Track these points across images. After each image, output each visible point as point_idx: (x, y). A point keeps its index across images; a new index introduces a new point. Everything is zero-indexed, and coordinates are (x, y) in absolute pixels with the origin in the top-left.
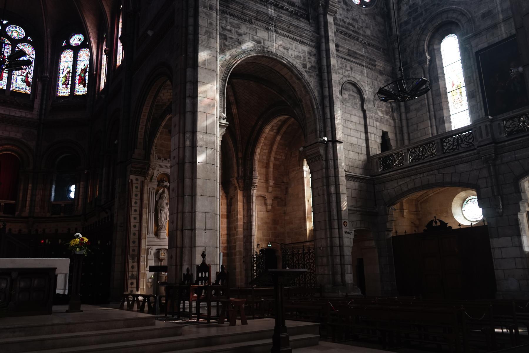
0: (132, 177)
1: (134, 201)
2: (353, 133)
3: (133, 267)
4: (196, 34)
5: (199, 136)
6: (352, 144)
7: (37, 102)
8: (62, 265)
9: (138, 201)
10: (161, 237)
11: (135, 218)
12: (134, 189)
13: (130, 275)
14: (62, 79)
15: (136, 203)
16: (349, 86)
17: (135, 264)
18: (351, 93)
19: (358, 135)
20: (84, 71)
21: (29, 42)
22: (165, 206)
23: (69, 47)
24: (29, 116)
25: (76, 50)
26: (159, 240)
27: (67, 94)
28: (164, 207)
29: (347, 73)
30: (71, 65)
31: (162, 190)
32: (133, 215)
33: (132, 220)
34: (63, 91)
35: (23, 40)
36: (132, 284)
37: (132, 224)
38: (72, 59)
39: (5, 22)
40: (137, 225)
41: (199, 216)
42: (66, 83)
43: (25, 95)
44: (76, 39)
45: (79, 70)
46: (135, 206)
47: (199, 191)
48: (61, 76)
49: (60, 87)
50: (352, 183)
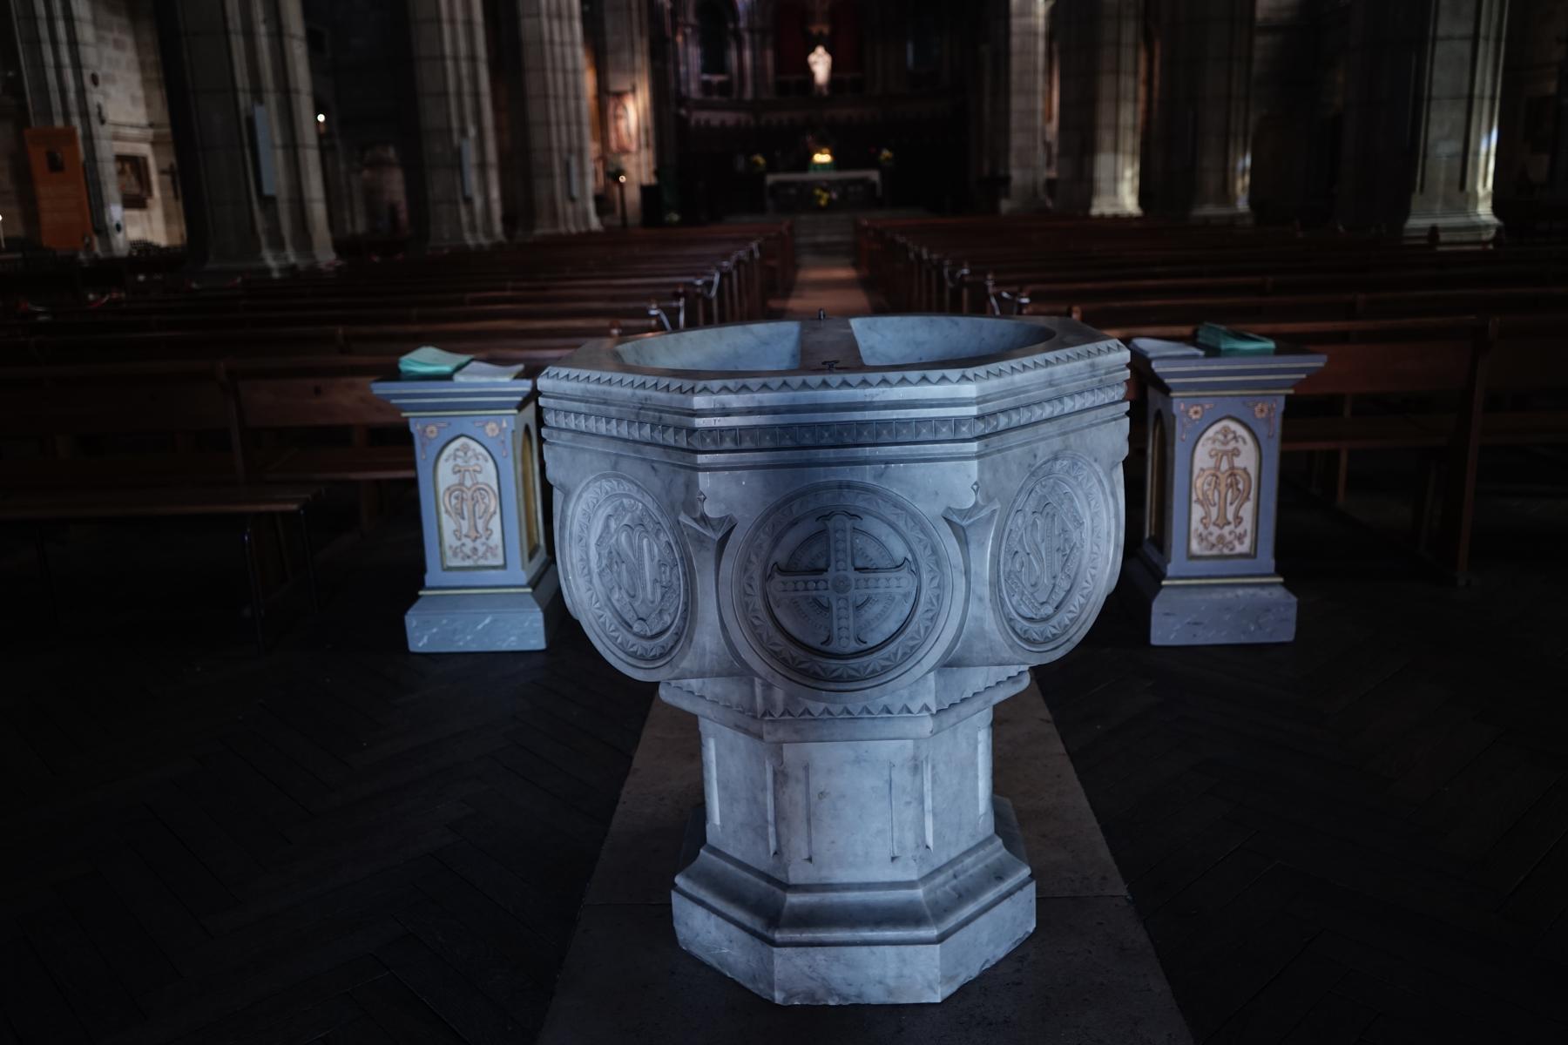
8: (874, 175)
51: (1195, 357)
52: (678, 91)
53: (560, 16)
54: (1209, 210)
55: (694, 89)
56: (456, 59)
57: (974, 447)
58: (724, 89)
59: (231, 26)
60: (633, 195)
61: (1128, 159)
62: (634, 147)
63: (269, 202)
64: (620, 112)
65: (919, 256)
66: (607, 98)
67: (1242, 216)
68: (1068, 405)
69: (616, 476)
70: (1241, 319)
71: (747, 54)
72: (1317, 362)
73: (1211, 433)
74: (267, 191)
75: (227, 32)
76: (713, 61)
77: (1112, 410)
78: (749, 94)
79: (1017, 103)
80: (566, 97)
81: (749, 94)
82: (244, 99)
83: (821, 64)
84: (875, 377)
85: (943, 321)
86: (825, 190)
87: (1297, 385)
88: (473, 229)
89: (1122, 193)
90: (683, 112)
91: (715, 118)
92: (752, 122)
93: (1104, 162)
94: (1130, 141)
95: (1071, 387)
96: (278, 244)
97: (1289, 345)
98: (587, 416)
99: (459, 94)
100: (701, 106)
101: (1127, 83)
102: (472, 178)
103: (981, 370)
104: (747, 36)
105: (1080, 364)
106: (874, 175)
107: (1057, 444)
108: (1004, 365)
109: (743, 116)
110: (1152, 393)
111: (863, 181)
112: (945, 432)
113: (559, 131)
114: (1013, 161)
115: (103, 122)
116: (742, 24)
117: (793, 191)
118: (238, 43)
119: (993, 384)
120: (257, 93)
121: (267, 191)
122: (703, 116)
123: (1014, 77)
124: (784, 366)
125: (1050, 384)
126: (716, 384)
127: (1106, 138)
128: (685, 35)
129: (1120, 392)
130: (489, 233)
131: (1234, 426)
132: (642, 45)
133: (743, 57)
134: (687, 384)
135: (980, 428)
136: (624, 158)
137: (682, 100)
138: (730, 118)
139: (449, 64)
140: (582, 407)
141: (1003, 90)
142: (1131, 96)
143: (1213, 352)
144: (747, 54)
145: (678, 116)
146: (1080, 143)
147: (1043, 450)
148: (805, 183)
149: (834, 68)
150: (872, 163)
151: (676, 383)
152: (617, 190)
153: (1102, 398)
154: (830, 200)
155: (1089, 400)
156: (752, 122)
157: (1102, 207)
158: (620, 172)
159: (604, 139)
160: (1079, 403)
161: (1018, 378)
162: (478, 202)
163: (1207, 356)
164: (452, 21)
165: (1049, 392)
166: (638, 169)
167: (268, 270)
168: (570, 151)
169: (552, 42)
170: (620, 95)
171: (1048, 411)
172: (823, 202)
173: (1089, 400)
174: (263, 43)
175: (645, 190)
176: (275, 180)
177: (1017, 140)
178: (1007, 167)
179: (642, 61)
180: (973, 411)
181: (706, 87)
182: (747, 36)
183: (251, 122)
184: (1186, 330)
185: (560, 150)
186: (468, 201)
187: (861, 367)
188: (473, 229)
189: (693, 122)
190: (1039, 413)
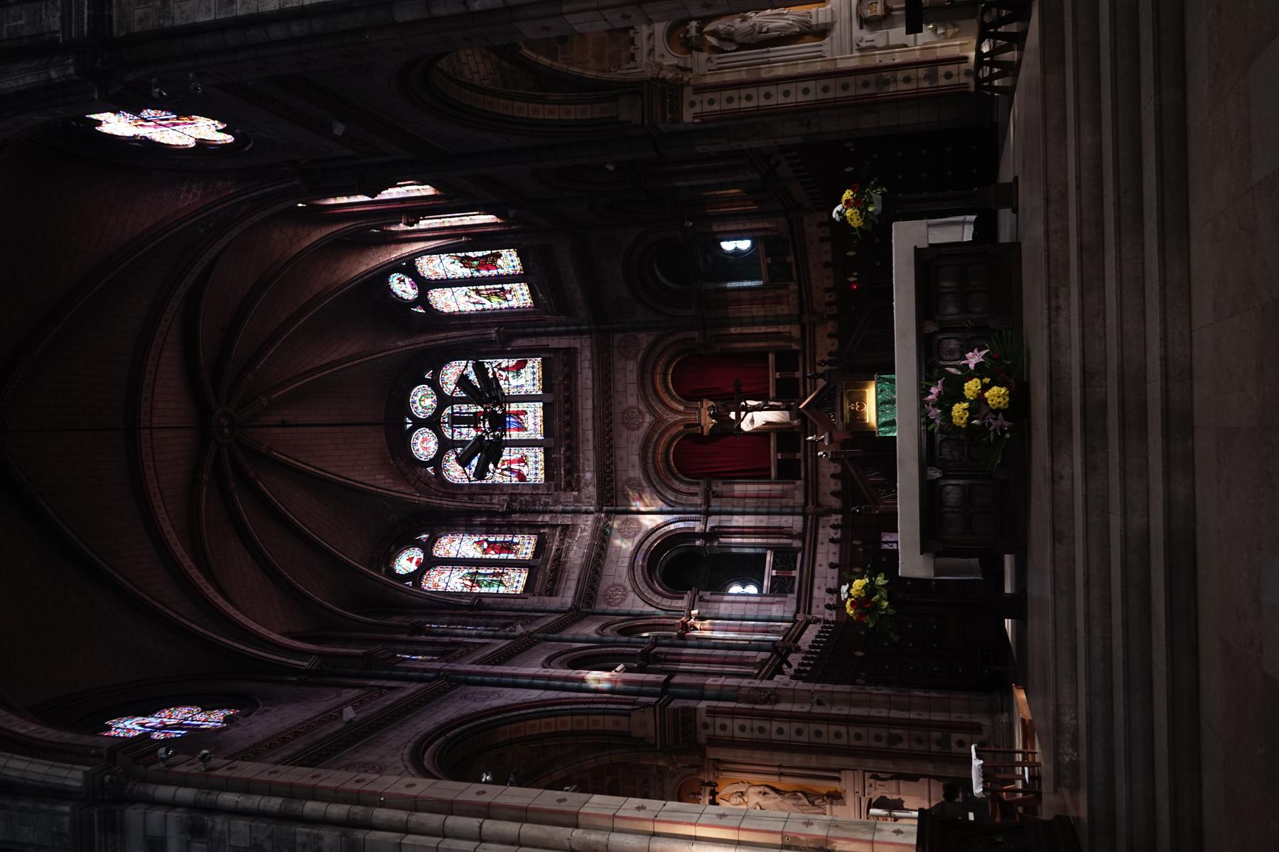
0: (688, 116)
1: (745, 104)
3: (907, 80)
7: (554, 343)
8: (907, 237)
9: (744, 92)
10: (829, 20)
11: (787, 94)
12: (716, 107)
13: (926, 84)
14: (495, 304)
15: (749, 98)
17: (900, 75)
20: (466, 262)
22: (750, 22)
23: (422, 299)
24: (587, 353)
25: (425, 285)
26: (837, 26)
27: (525, 287)
28: (753, 26)
31: (709, 38)
32: (778, 99)
33: (791, 99)
34: (520, 296)
36: (948, 75)
37: (801, 98)
38: (448, 290)
40: (802, 85)
43: (545, 367)
44: (403, 288)
45: (466, 272)
46: (758, 99)
48: (488, 305)
49: (514, 303)
55: (781, 609)
58: (785, 558)
71: (738, 521)
78: (795, 522)
81: (795, 522)
86: (954, 393)
92: (836, 519)
100: (805, 601)
104: (713, 521)
115: (929, 226)
116: (698, 527)
117: (952, 491)
133: (742, 525)
144: (738, 521)
148: (928, 456)
150: (875, 242)
154: (990, 373)
156: (836, 519)
172: (997, 395)
181: (780, 587)
182: (713, 521)
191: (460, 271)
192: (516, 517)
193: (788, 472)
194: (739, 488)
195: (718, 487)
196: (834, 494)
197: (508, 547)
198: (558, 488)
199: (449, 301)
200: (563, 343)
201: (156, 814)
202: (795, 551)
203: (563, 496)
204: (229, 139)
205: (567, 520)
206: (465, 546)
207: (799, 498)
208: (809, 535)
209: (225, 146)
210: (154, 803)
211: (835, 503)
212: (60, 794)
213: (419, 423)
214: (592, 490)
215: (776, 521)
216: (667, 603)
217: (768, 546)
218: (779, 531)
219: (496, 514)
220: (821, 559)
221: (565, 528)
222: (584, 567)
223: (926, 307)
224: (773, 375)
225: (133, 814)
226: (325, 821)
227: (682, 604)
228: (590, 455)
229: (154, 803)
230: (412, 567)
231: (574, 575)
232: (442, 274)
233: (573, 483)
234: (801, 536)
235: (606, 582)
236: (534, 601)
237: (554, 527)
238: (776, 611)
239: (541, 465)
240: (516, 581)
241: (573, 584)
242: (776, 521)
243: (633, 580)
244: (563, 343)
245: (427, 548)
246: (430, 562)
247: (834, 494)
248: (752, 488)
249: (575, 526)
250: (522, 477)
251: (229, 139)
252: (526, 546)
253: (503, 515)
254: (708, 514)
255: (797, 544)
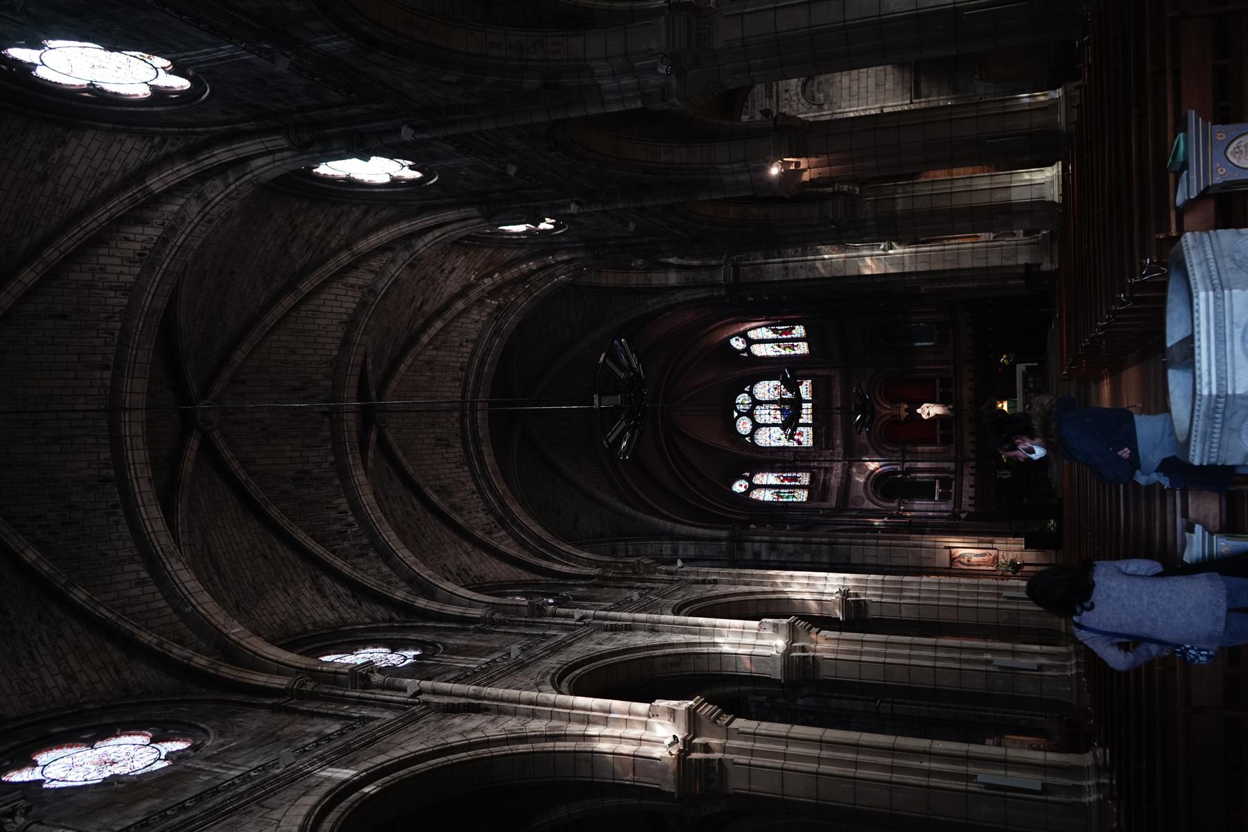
2: (863, 85)
4: (815, 279)
5: (907, 270)
6: (877, 85)
7: (819, 373)
8: (1020, 368)
14: (788, 352)
16: (808, 93)
18: (815, 88)
19: (864, 76)
20: (775, 331)
21: (751, 389)
23: (747, 350)
24: (838, 378)
25: (750, 342)
27: (806, 344)
29: (795, 98)
30: (768, 346)
34: (803, 348)
35: (751, 394)
38: (762, 346)
39: (736, 414)
41: (977, 264)
42: (792, 347)
43: (813, 384)
44: (738, 344)
45: (775, 336)
47: (956, 266)
48: (783, 352)
49: (798, 352)
50: (924, 88)
51: (1188, 175)
52: (948, 518)
53: (901, 590)
54: (1061, 118)
56: (936, 659)
57: (1226, 292)
58: (945, 484)
59: (925, 783)
60: (1030, 556)
61: (1016, 178)
62: (993, 552)
63: (1046, 789)
64: (965, 560)
65: (1103, 328)
66: (953, 568)
67: (1066, 93)
68: (1210, 256)
69: (1240, 430)
70: (1163, 150)
71: (920, 465)
72: (1192, 114)
73: (1234, 161)
74: (1039, 788)
75: (928, 787)
76: (925, 491)
77: (1213, 238)
78: (951, 465)
79: (966, 263)
80: (958, 593)
81: (951, 465)
82: (972, 787)
83: (929, 410)
84: (1196, 329)
85: (1169, 306)
87: (1205, 121)
88: (1063, 668)
89: (1045, 179)
90: (963, 516)
91: (968, 492)
92: (972, 464)
93: (1017, 196)
94: (1002, 179)
95: (1202, 255)
96: (1079, 790)
97: (1181, 125)
98: (1210, 452)
99: (961, 661)
101: (959, 186)
102: (1024, 662)
103: (1194, 291)
104: (907, 465)
105: (1192, 253)
106: (1020, 368)
107: (1227, 259)
108: (1192, 282)
109: (967, 471)
110: (1210, 192)
111: (1025, 377)
112: (1220, 303)
113: (982, 601)
114: (1011, 262)
118: (934, 782)
119: (1200, 286)
120: (968, 778)
121: (1039, 788)
122: (965, 500)
123: (947, 267)
124: (1191, 375)
125: (1200, 264)
126: (1198, 387)
127: (999, 197)
128: (904, 511)
129: (1205, 235)
130: (1067, 656)
131: (1231, 149)
132: (916, 539)
133: (923, 468)
134: (1198, 397)
135: (1218, 290)
136: (1001, 560)
137: (955, 516)
138: (968, 481)
139: (939, 664)
140: (1208, 444)
141: (957, 274)
142: (968, 182)
143: (1185, 165)
144: (920, 465)
145: (966, 519)
146: (1001, 216)
147: (1230, 265)
149: (933, 401)
151: (1197, 402)
152: (1026, 568)
153: (1207, 243)
155: (1208, 248)
156: (972, 464)
157: (1054, 194)
158: (1013, 563)
159: (986, 574)
160: (1209, 252)
161: (1198, 277)
162: (1043, 661)
163: (1187, 168)
164: (910, 657)
165: (1204, 265)
166: (1010, 550)
167: (1099, 800)
168: (999, 595)
169: (918, 598)
170: (952, 559)
171: (1212, 264)
173: (1208, 248)
174: (935, 766)
175: (1028, 546)
176: (1032, 781)
177: (995, 261)
178: (1017, 266)
179: (928, 540)
180: (1211, 293)
181: (944, 497)
182: (907, 465)
183: (989, 786)
184: (1172, 176)
185: (998, 602)
186: (1040, 667)
187: (1192, 336)
188: (1063, 668)
189: (972, 509)
190: (1213, 268)
191: (771, 335)
192: (798, 463)
193: (946, 440)
194: (920, 449)
195: (909, 448)
196: (972, 451)
197: (795, 479)
198: (821, 448)
199: (759, 350)
200: (825, 373)
201: (757, 545)
202: (950, 480)
203: (824, 453)
204: (417, 175)
205: (827, 465)
206: (771, 479)
207: (953, 453)
208: (959, 473)
209: (183, 94)
210: (753, 541)
211: (972, 456)
212: (718, 539)
213: (741, 414)
214: (840, 450)
215: (941, 465)
216: (885, 504)
217: (936, 478)
218: (943, 470)
219: (789, 461)
220: (965, 483)
221: (826, 469)
222: (839, 488)
223: (1025, 385)
224: (939, 390)
225: (748, 545)
226: (821, 543)
227: (894, 505)
228: (839, 431)
229: (753, 541)
230: (743, 490)
231: (835, 492)
232: (760, 337)
233: (830, 446)
234: (954, 472)
235: (852, 495)
236: (814, 505)
237: (820, 468)
238: (943, 507)
239: (811, 436)
240: (802, 496)
241: (835, 496)
242: (941, 465)
243: (867, 494)
244: (825, 373)
245: (749, 480)
246: (753, 487)
247: (972, 451)
248: (927, 449)
249: (832, 468)
250: (799, 442)
251: (417, 175)
252: (805, 479)
253: (791, 462)
254: (904, 461)
255: (952, 476)
